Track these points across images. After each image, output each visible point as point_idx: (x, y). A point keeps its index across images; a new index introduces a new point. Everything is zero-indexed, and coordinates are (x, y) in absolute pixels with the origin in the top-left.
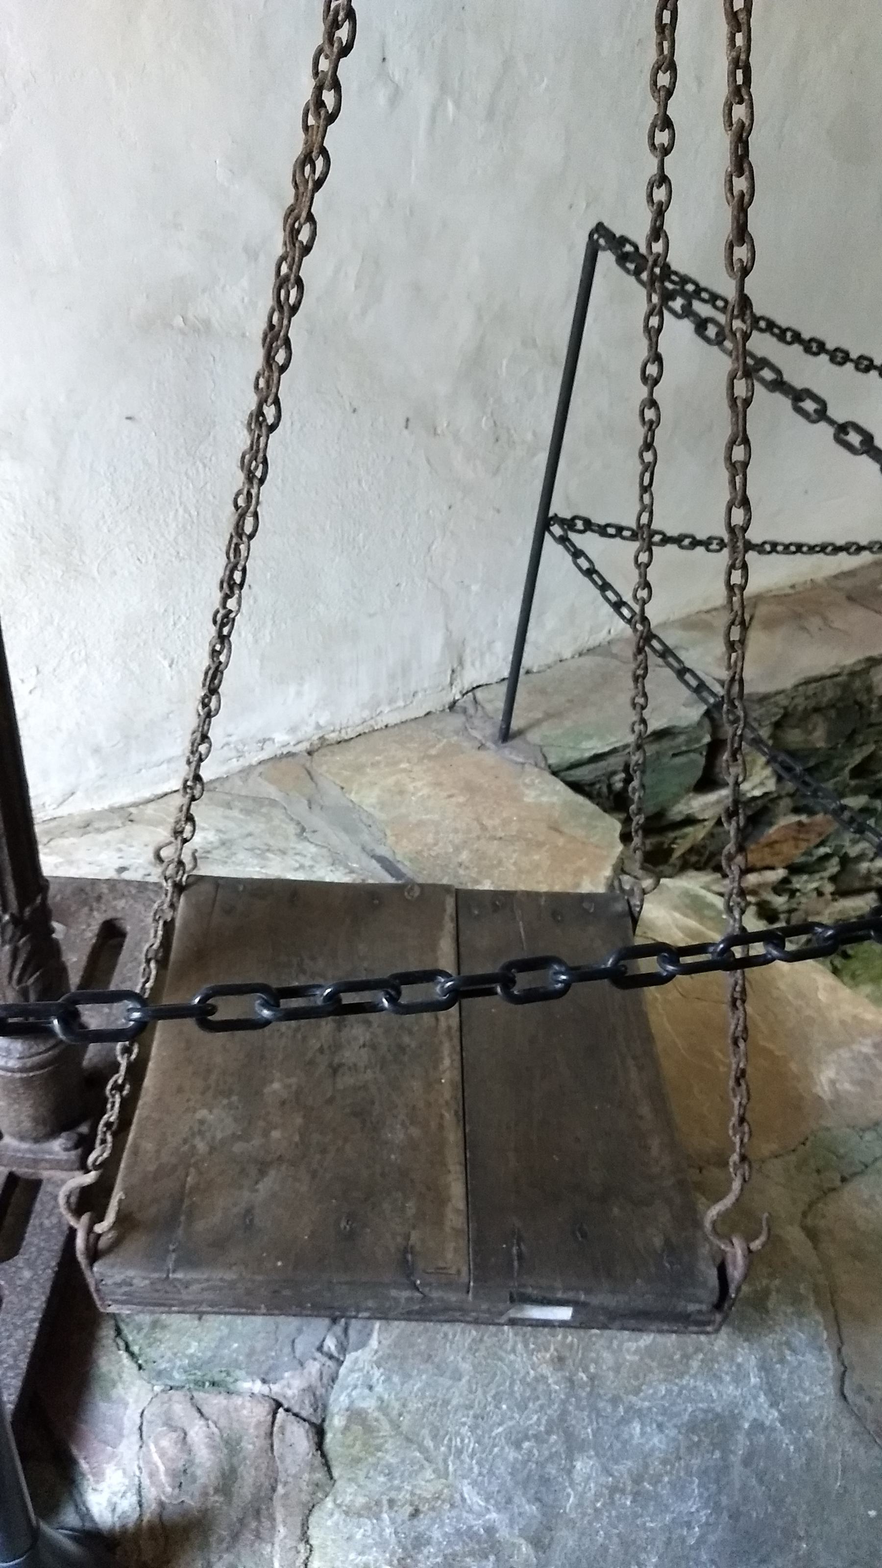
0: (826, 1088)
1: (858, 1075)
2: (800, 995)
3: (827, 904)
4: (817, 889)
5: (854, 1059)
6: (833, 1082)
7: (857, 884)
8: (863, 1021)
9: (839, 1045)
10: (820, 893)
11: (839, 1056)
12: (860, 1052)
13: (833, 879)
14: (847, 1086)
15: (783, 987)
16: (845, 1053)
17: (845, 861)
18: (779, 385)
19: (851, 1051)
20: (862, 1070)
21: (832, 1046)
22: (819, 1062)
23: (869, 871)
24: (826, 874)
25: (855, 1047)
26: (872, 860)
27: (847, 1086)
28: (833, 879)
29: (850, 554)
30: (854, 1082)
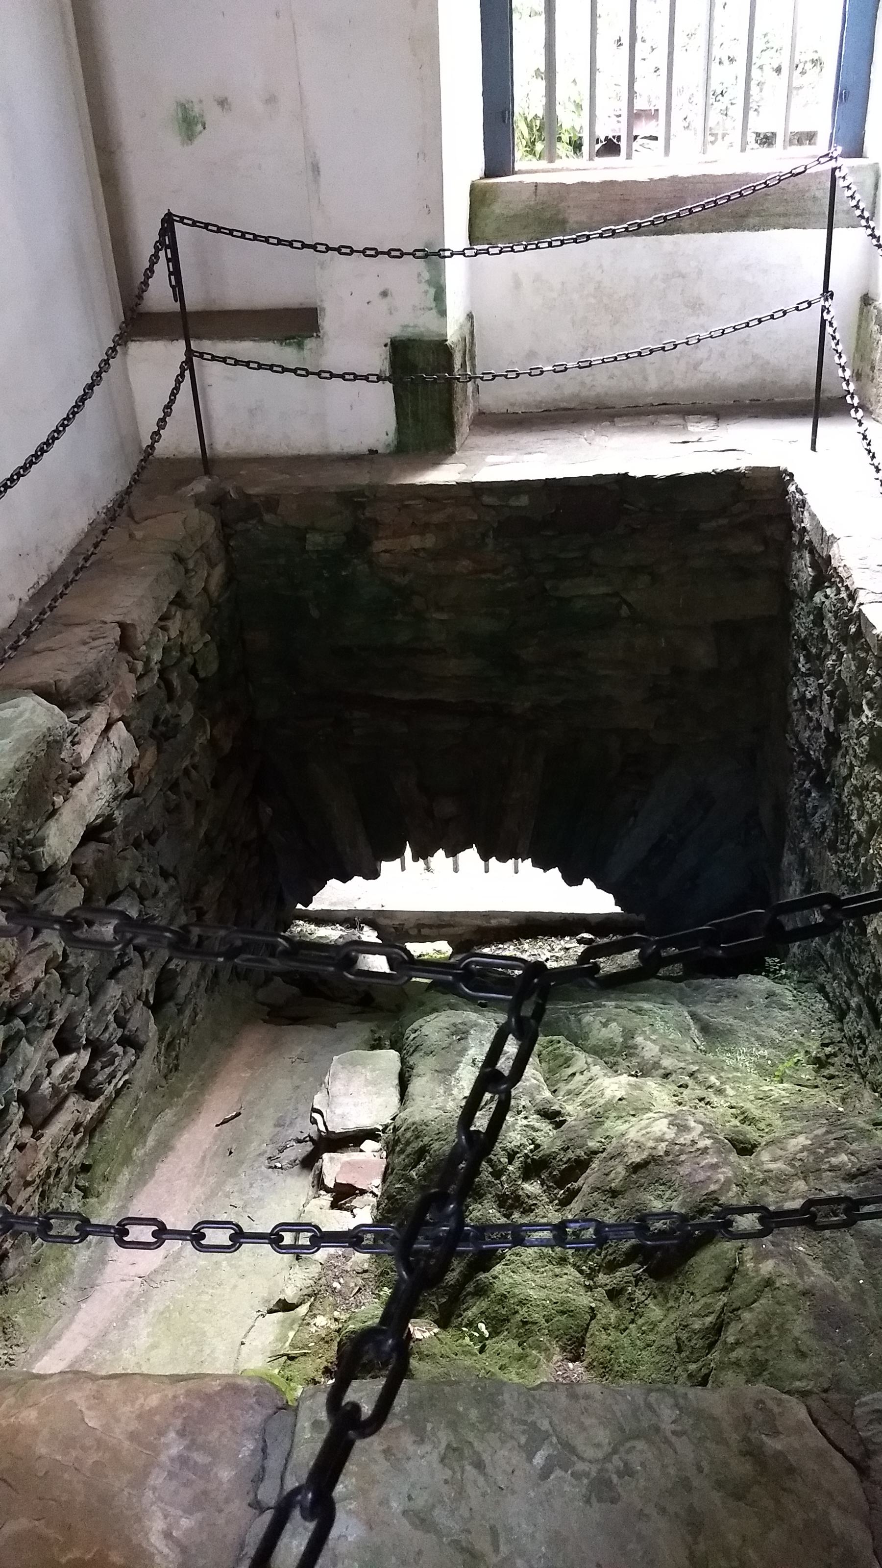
0: (166, 1551)
1: (186, 1495)
2: (69, 1443)
3: (36, 1149)
4: (15, 1146)
5: (171, 1475)
6: (167, 1535)
7: (51, 1106)
8: (153, 1412)
9: (145, 1473)
10: (20, 1147)
11: (154, 1489)
12: (172, 1460)
13: (24, 1123)
14: (185, 1523)
15: (43, 1450)
16: (157, 1478)
17: (23, 1099)
18: (214, 358)
19: (161, 1466)
20: (188, 1484)
21: (139, 1481)
22: (139, 1520)
23: (53, 1085)
24: (15, 1126)
25: (163, 1458)
26: (49, 1074)
27: (185, 1523)
28: (24, 1123)
29: (156, 263)
30: (188, 1511)
